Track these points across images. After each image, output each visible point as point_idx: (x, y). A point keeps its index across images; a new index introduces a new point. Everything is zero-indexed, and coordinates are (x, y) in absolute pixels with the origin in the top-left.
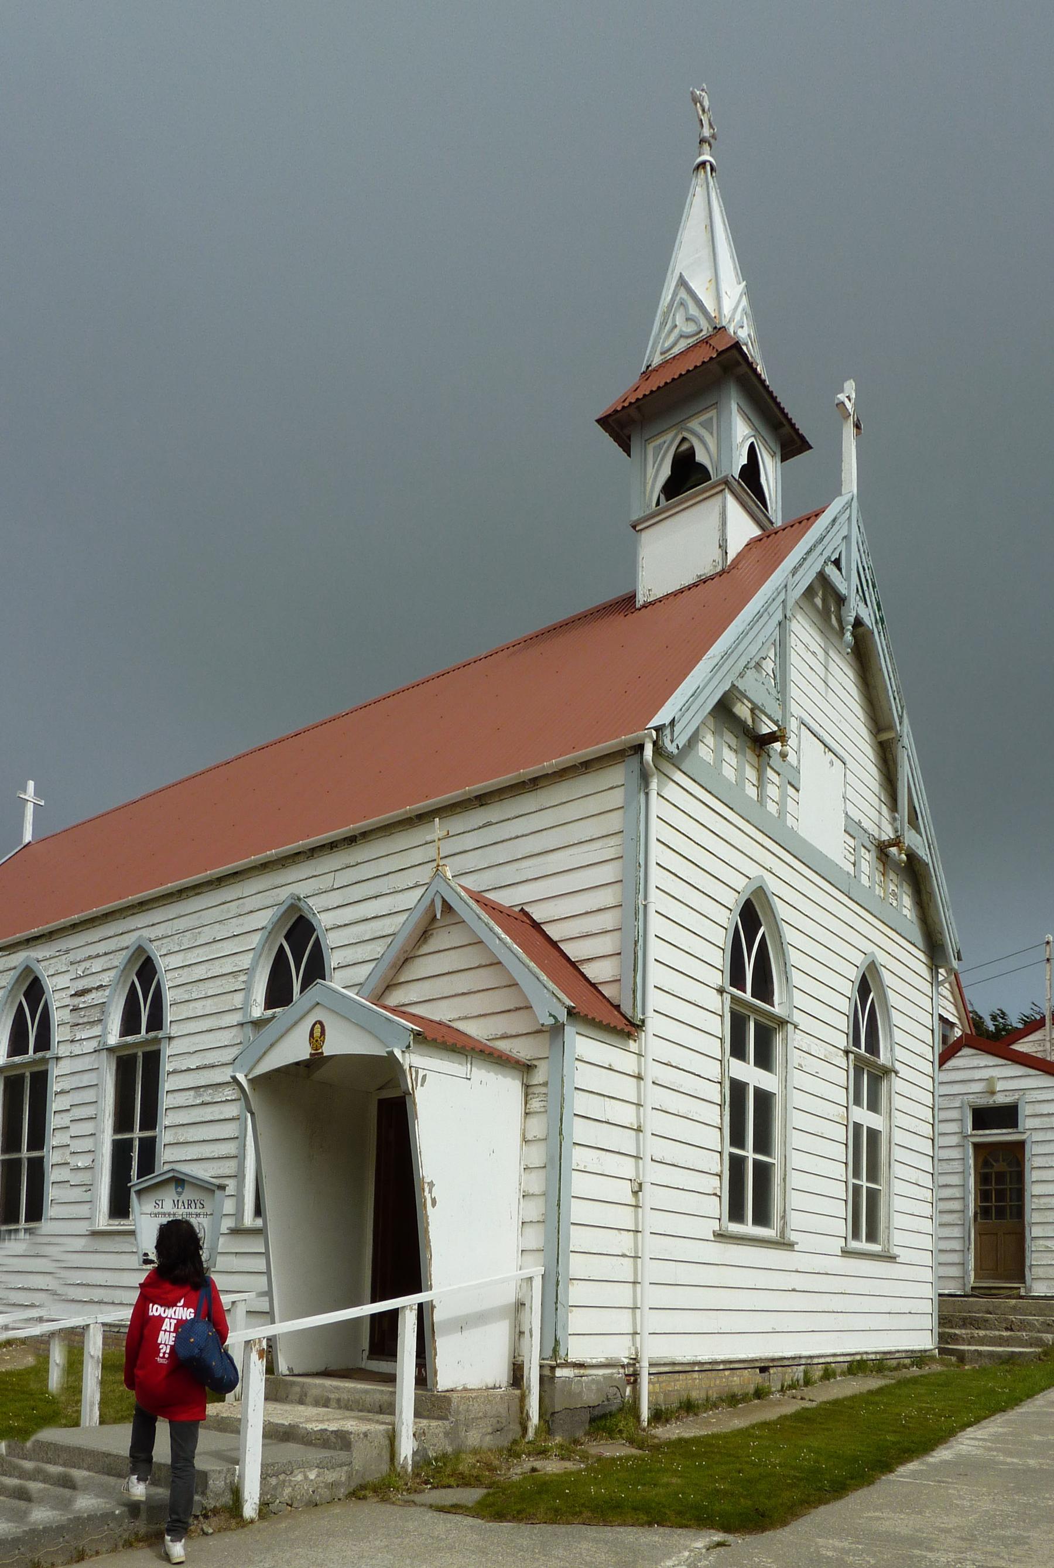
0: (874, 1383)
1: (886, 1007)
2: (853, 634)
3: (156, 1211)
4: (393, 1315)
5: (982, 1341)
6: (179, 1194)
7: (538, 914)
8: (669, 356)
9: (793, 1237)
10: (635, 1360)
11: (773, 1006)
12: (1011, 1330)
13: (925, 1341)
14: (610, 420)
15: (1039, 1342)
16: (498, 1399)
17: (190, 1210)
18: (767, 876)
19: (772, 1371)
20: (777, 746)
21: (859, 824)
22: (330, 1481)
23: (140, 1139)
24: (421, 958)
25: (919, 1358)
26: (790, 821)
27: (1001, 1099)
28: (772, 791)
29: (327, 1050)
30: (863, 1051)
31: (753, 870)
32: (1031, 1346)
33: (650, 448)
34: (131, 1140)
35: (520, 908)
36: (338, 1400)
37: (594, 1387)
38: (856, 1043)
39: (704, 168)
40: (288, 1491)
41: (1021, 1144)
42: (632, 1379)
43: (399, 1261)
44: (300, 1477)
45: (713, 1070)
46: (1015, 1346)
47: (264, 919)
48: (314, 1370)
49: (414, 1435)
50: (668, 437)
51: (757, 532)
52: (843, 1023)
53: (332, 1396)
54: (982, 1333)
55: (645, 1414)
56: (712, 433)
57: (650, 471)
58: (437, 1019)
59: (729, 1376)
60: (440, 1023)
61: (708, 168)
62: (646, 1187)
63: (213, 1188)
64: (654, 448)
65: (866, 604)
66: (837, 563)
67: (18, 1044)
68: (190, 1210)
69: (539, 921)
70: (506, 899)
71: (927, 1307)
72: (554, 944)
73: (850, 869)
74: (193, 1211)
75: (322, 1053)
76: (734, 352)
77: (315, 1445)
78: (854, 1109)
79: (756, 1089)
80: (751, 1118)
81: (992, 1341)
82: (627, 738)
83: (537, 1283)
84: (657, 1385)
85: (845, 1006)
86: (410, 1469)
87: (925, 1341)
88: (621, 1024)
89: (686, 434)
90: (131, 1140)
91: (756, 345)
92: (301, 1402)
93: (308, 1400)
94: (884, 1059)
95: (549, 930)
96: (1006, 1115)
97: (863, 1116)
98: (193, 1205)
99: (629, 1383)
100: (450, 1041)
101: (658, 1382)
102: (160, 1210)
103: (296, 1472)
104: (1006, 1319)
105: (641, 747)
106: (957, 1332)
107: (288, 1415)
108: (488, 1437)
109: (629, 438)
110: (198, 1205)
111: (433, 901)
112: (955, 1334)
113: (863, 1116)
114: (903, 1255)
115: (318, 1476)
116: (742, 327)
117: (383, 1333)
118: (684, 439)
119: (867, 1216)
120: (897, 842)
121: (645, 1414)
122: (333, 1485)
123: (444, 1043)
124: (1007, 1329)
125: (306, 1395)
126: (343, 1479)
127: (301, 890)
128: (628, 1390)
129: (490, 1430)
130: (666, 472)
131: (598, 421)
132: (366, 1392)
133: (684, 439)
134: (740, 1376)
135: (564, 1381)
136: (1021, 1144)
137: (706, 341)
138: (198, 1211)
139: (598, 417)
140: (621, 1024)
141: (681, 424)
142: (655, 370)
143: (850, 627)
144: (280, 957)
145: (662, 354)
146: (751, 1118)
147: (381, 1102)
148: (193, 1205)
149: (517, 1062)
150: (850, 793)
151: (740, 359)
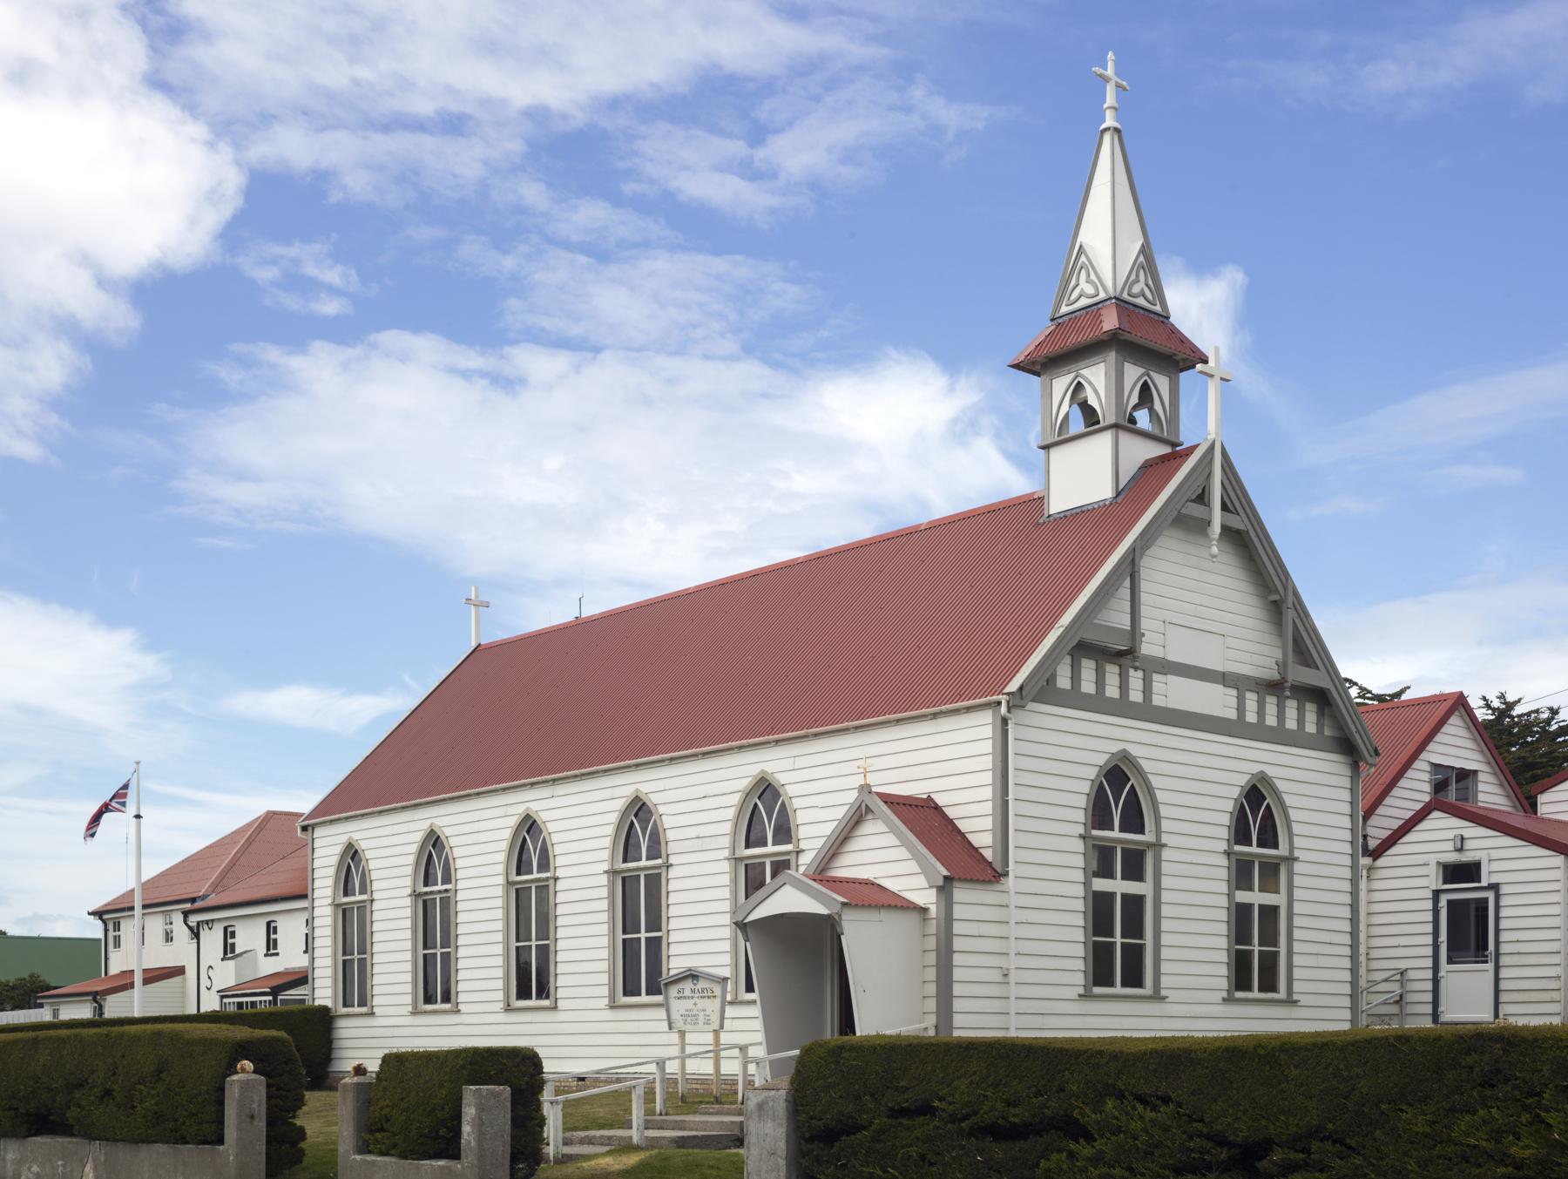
23: (1250, 953)
114: (1304, 1000)
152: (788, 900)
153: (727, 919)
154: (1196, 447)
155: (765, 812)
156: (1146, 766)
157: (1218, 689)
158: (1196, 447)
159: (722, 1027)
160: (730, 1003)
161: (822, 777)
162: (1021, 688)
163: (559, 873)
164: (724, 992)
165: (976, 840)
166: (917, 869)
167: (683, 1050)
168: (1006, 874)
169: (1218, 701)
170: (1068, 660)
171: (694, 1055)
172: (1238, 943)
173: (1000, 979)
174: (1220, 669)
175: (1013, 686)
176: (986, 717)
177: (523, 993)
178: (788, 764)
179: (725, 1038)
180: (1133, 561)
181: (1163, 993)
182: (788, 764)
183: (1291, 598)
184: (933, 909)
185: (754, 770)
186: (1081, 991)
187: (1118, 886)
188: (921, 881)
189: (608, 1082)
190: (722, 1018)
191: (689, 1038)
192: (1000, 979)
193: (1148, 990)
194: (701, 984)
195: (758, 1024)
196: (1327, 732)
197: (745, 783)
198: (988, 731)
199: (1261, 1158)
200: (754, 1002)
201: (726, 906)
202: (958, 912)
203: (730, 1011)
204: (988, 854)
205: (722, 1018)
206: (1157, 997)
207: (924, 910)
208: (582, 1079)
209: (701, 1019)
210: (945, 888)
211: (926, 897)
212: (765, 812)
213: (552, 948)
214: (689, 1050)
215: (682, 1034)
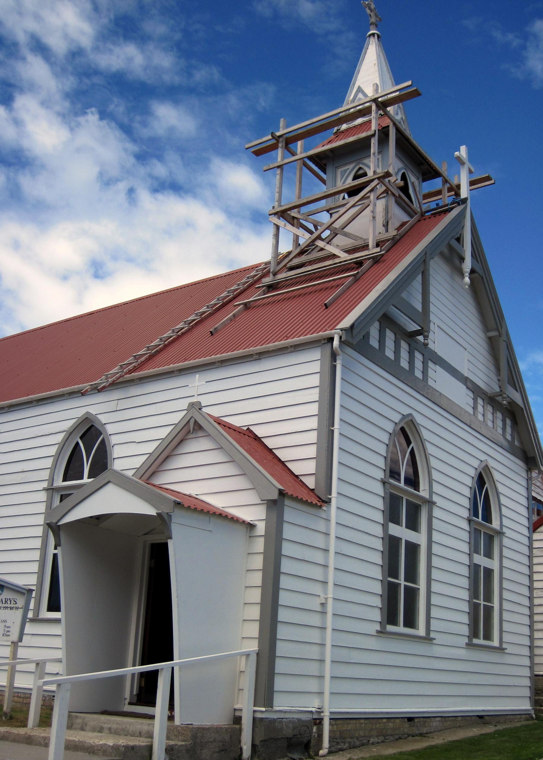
0: (490, 729)
4: (155, 674)
7: (259, 431)
9: (432, 635)
10: (320, 711)
11: (419, 492)
13: (525, 705)
16: (224, 730)
19: (416, 720)
20: (421, 338)
24: (181, 456)
26: (430, 383)
28: (418, 364)
30: (480, 520)
33: (339, 171)
35: (247, 428)
36: (110, 729)
37: (291, 725)
38: (476, 515)
39: (374, 36)
42: (318, 721)
43: (158, 643)
45: (379, 531)
49: (166, 750)
50: (351, 166)
52: (466, 503)
53: (105, 726)
58: (188, 493)
59: (385, 722)
60: (190, 496)
61: (376, 37)
63: (24, 591)
64: (341, 172)
65: (478, 262)
69: (260, 436)
70: (237, 422)
72: (270, 451)
73: (471, 411)
74: (9, 605)
78: (475, 556)
79: (407, 542)
83: (254, 658)
84: (335, 727)
85: (467, 492)
88: (315, 501)
89: (361, 166)
90: (405, 586)
91: (406, 123)
92: (82, 729)
93: (88, 728)
94: (495, 524)
95: (266, 441)
97: (480, 560)
98: (9, 602)
99: (315, 724)
100: (199, 508)
101: (336, 724)
105: (331, 339)
107: (77, 736)
108: (216, 755)
109: (325, 165)
110: (12, 602)
111: (189, 421)
113: (480, 560)
114: (510, 649)
116: (397, 114)
117: (148, 682)
118: (360, 168)
119: (480, 622)
120: (501, 393)
123: (196, 509)
125: (86, 725)
127: (93, 410)
128: (315, 729)
129: (217, 750)
133: (360, 168)
134: (394, 723)
135: (270, 721)
138: (12, 605)
140: (315, 501)
143: (467, 274)
146: (400, 563)
148: (9, 602)
149: (244, 522)
152: (110, 501)
153: (41, 520)
155: (87, 453)
156: (425, 434)
157: (462, 388)
159: (20, 640)
160: (32, 620)
161: (137, 424)
162: (352, 326)
164: (26, 609)
165: (296, 468)
166: (248, 485)
168: (328, 502)
169: (461, 396)
170: (377, 325)
173: (319, 608)
174: (466, 375)
175: (347, 322)
176: (316, 354)
178: (112, 406)
179: (22, 653)
180: (424, 261)
181: (432, 635)
182: (112, 406)
183: (504, 337)
184: (261, 528)
185: (80, 413)
186: (378, 628)
187: (400, 531)
188: (252, 497)
190: (22, 634)
192: (319, 608)
193: (421, 631)
195: (59, 642)
196: (516, 443)
197: (68, 425)
198: (316, 367)
201: (42, 508)
202: (288, 532)
203: (29, 628)
204: (310, 482)
205: (22, 634)
206: (428, 639)
207: (251, 526)
210: (275, 505)
211: (255, 514)
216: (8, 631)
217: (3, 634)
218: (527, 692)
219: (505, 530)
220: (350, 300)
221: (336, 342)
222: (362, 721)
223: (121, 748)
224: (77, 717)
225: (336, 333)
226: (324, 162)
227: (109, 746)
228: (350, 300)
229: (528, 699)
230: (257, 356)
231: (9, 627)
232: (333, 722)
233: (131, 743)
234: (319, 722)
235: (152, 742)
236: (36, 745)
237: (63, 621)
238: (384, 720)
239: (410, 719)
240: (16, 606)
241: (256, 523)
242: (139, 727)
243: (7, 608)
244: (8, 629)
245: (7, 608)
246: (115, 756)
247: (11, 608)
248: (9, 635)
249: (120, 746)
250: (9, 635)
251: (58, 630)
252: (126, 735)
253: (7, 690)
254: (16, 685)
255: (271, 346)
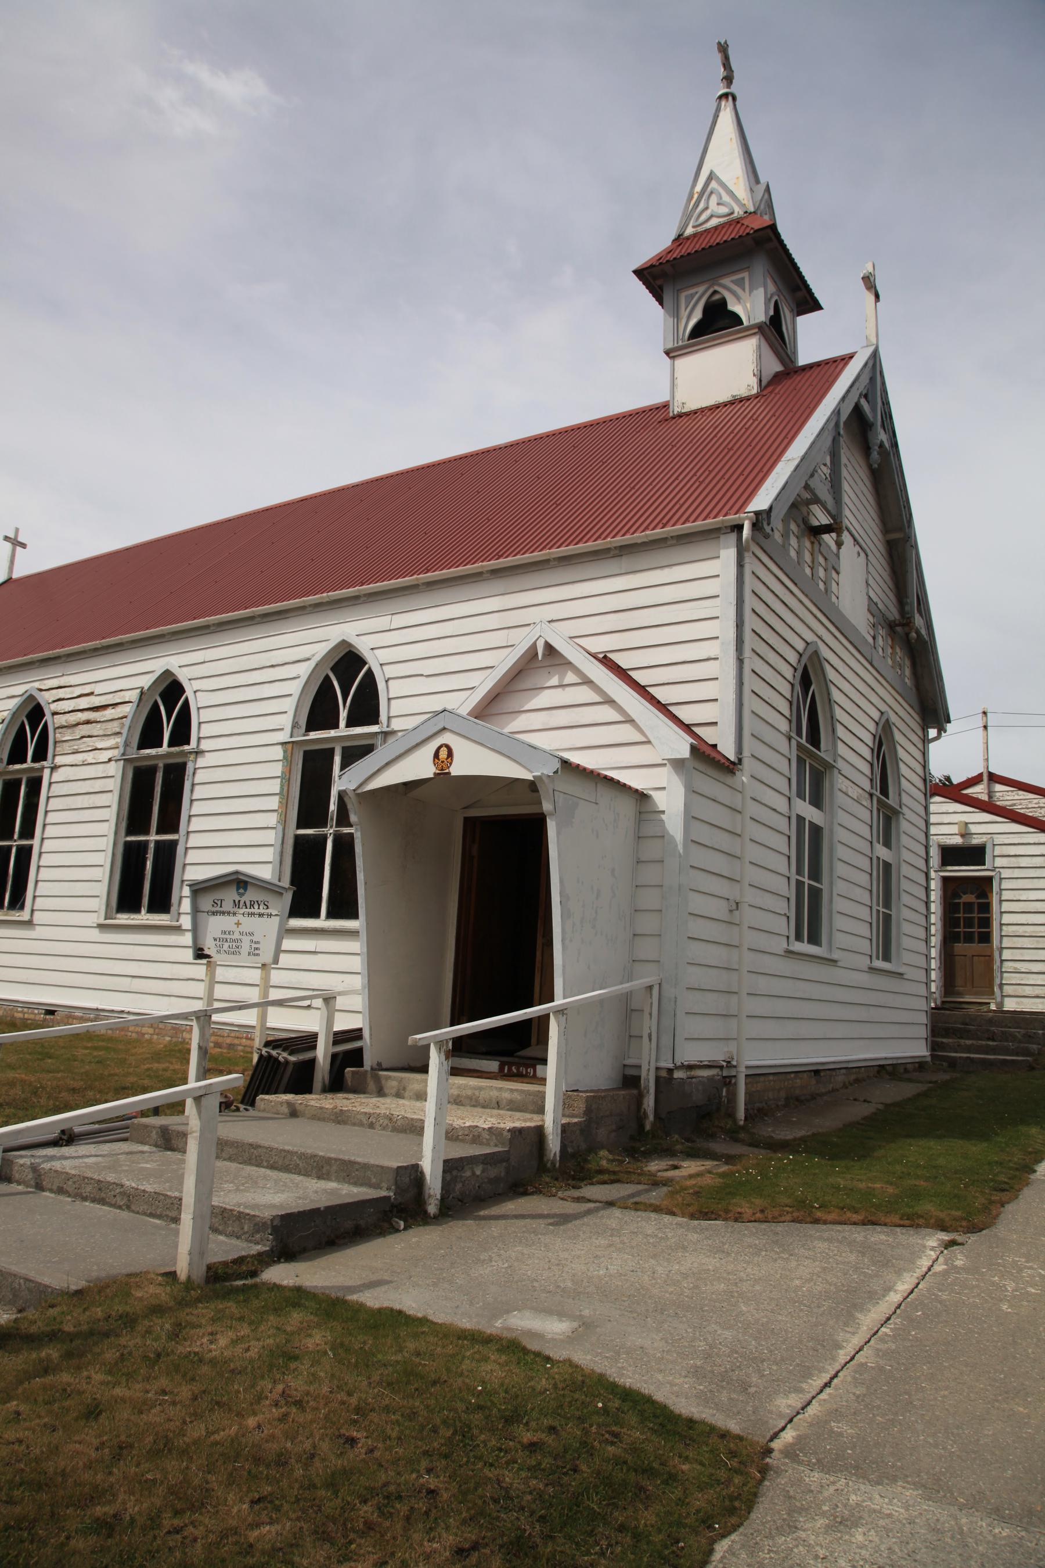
1: (896, 760)
2: (879, 453)
3: (214, 909)
5: (969, 1049)
6: (241, 895)
8: (700, 229)
12: (993, 1040)
13: (920, 1050)
14: (645, 272)
15: (1027, 1053)
17: (252, 910)
18: (820, 643)
21: (876, 604)
22: (492, 1176)
23: (157, 842)
25: (920, 1065)
27: (976, 841)
29: (456, 769)
31: (810, 637)
32: (1017, 1055)
33: (683, 296)
34: (147, 842)
37: (700, 1088)
40: (459, 1186)
41: (989, 880)
44: (468, 1174)
46: (999, 1054)
47: (321, 650)
48: (400, 1065)
50: (701, 289)
51: (778, 367)
54: (969, 1042)
55: (741, 1114)
56: (744, 290)
57: (684, 314)
62: (745, 908)
64: (686, 297)
66: (866, 396)
67: (17, 754)
68: (252, 910)
71: (923, 1019)
73: (870, 640)
74: (256, 911)
75: (449, 773)
76: (769, 231)
77: (462, 1141)
80: (812, 846)
81: (979, 1050)
82: (732, 518)
86: (557, 1165)
87: (920, 1050)
89: (717, 288)
92: (399, 1095)
96: (975, 854)
97: (882, 852)
98: (256, 906)
102: (218, 909)
103: (466, 1168)
104: (988, 1030)
105: (739, 528)
106: (944, 1040)
112: (942, 1043)
115: (483, 1171)
118: (715, 292)
121: (741, 1114)
122: (495, 1181)
124: (989, 1039)
125: (404, 1089)
126: (503, 1174)
129: (614, 1127)
130: (697, 316)
131: (636, 272)
132: (480, 1089)
133: (715, 292)
136: (989, 880)
137: (738, 221)
138: (262, 911)
139: (634, 268)
141: (714, 281)
142: (688, 238)
143: (876, 448)
144: (325, 687)
145: (694, 227)
146: (812, 846)
147: (466, 819)
148: (256, 906)
150: (871, 581)
151: (773, 237)
154: (851, 357)
155: (346, 690)
158: (851, 357)
159: (276, 961)
163: (205, 745)
167: (266, 994)
171: (280, 1003)
172: (130, 832)
177: (127, 899)
189: (82, 1020)
190: (278, 951)
191: (221, 973)
194: (250, 895)
195: (357, 963)
199: (388, 1198)
200: (353, 934)
202: (933, 808)
205: (278, 951)
208: (52, 1013)
209: (245, 947)
212: (346, 690)
213: (123, 832)
214: (274, 995)
215: (211, 966)
216: (257, 949)
217: (249, 954)
218: (923, 1032)
219: (905, 810)
220: (746, 473)
221: (746, 532)
222: (771, 1078)
223: (505, 1133)
224: (388, 1078)
225: (747, 518)
226: (659, 282)
227: (484, 1129)
228: (727, 477)
229: (924, 1041)
230: (617, 552)
231: (258, 943)
232: (749, 1080)
233: (518, 1124)
234: (728, 1082)
235: (543, 1120)
236: (354, 1124)
237: (363, 935)
238: (792, 1075)
239: (817, 1072)
240: (269, 911)
241: (651, 793)
242: (495, 1094)
243: (253, 914)
244: (257, 946)
245: (253, 914)
246: (496, 1146)
247: (261, 915)
248: (258, 955)
249: (503, 1129)
250: (258, 955)
251: (355, 946)
252: (474, 1106)
253: (258, 1029)
254: (269, 1025)
255: (639, 537)
